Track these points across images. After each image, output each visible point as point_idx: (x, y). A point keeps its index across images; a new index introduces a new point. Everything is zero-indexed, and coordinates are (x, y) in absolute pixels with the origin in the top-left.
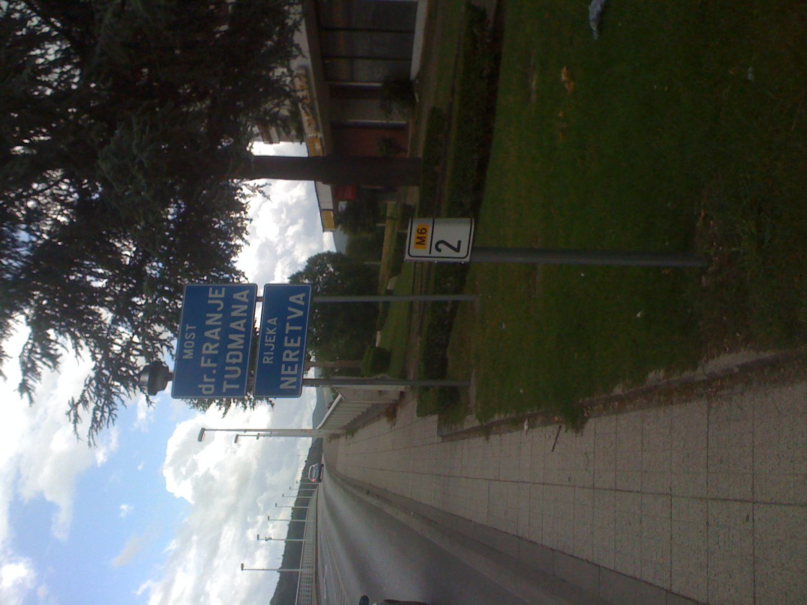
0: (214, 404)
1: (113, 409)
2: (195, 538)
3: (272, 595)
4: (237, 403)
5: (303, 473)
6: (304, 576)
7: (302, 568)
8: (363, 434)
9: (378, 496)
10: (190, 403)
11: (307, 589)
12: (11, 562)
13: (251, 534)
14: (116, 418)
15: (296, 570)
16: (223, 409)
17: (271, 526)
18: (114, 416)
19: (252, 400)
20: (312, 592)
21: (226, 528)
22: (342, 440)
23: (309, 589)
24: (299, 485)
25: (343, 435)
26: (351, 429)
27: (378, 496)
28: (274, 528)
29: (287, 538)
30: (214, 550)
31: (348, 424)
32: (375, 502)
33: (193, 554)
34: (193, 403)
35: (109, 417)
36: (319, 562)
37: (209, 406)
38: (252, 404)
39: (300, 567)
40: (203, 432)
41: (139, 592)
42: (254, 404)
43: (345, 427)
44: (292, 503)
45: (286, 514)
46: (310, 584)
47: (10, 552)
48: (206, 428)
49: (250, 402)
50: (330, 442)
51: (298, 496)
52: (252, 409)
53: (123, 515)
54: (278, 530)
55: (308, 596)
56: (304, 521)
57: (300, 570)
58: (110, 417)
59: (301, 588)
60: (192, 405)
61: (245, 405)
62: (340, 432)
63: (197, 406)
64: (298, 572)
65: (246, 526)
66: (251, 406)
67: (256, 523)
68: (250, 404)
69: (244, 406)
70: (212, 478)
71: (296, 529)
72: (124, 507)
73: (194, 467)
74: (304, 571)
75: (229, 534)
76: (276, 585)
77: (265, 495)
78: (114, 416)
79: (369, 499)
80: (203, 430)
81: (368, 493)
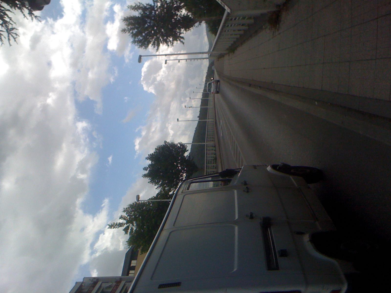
0: (150, 45)
1: (13, 29)
2: (159, 109)
3: (196, 126)
4: (163, 43)
5: (206, 78)
6: (209, 148)
7: (208, 119)
8: (242, 50)
9: (260, 87)
10: (137, 45)
11: (212, 128)
12: (79, 121)
13: (183, 105)
14: (17, 37)
15: (205, 120)
16: (156, 47)
17: (193, 101)
18: (14, 35)
19: (171, 41)
20: (214, 129)
21: (172, 103)
22: (226, 57)
23: (213, 128)
24: (205, 83)
25: (226, 54)
26: (232, 49)
27: (260, 87)
28: (194, 102)
29: (202, 98)
30: (168, 111)
31: (232, 44)
32: (258, 91)
33: (158, 114)
34: (139, 45)
35: (9, 36)
36: (217, 117)
37: (148, 46)
38: (171, 44)
39: (207, 118)
40: (141, 58)
41: (136, 131)
42: (173, 43)
43: (227, 49)
44: (202, 91)
45: (200, 96)
46: (213, 126)
47: (78, 118)
48: (142, 55)
49: (171, 42)
50: (218, 60)
51: (204, 87)
52: (172, 46)
53: (126, 101)
54: (197, 103)
55: (212, 135)
56: (207, 107)
57: (207, 120)
58: (10, 35)
59: (208, 155)
60: (138, 46)
61: (168, 44)
62: (225, 52)
63: (141, 47)
64: (206, 121)
65: (182, 102)
66: (171, 45)
67: (186, 101)
68: (170, 43)
69: (167, 44)
70: (163, 84)
71: (205, 102)
72: (126, 98)
73: (155, 79)
74: (210, 120)
75: (174, 105)
76: (197, 124)
77: (189, 90)
78: (14, 35)
79: (252, 89)
80: (140, 56)
81: (250, 85)
